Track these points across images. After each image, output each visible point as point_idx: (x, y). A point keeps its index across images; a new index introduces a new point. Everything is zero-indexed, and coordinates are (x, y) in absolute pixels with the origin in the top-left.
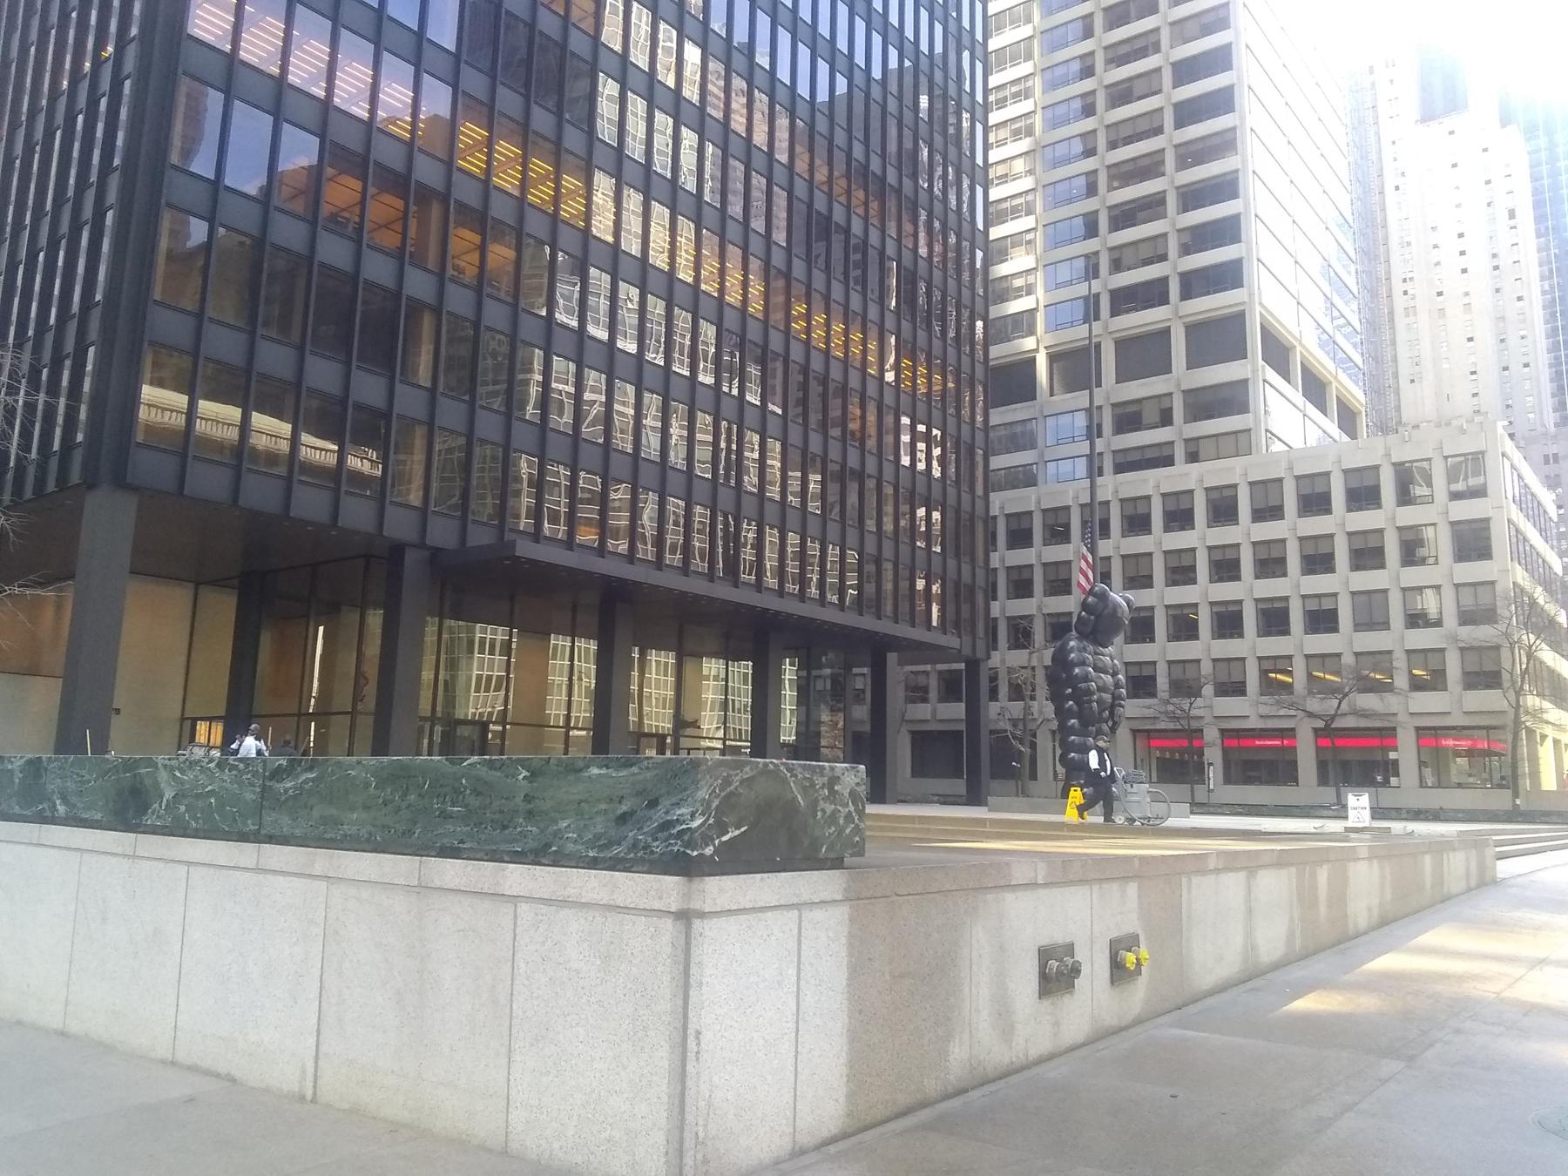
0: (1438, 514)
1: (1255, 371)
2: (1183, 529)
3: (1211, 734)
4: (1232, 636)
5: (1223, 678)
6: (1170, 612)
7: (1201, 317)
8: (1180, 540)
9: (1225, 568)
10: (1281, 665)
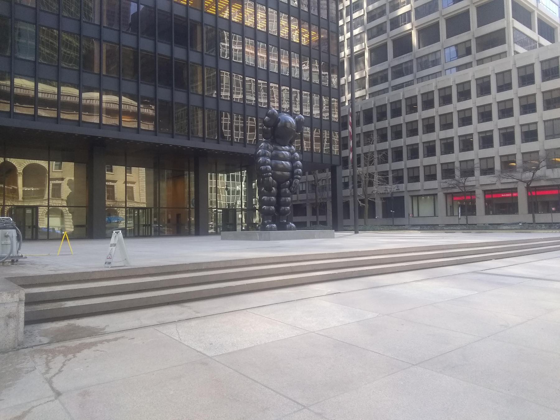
0: (514, 94)
1: (508, 23)
2: (466, 99)
3: (479, 194)
4: (488, 147)
5: (484, 167)
6: (461, 139)
7: (396, 37)
8: (448, 109)
9: (485, 116)
10: (511, 158)
